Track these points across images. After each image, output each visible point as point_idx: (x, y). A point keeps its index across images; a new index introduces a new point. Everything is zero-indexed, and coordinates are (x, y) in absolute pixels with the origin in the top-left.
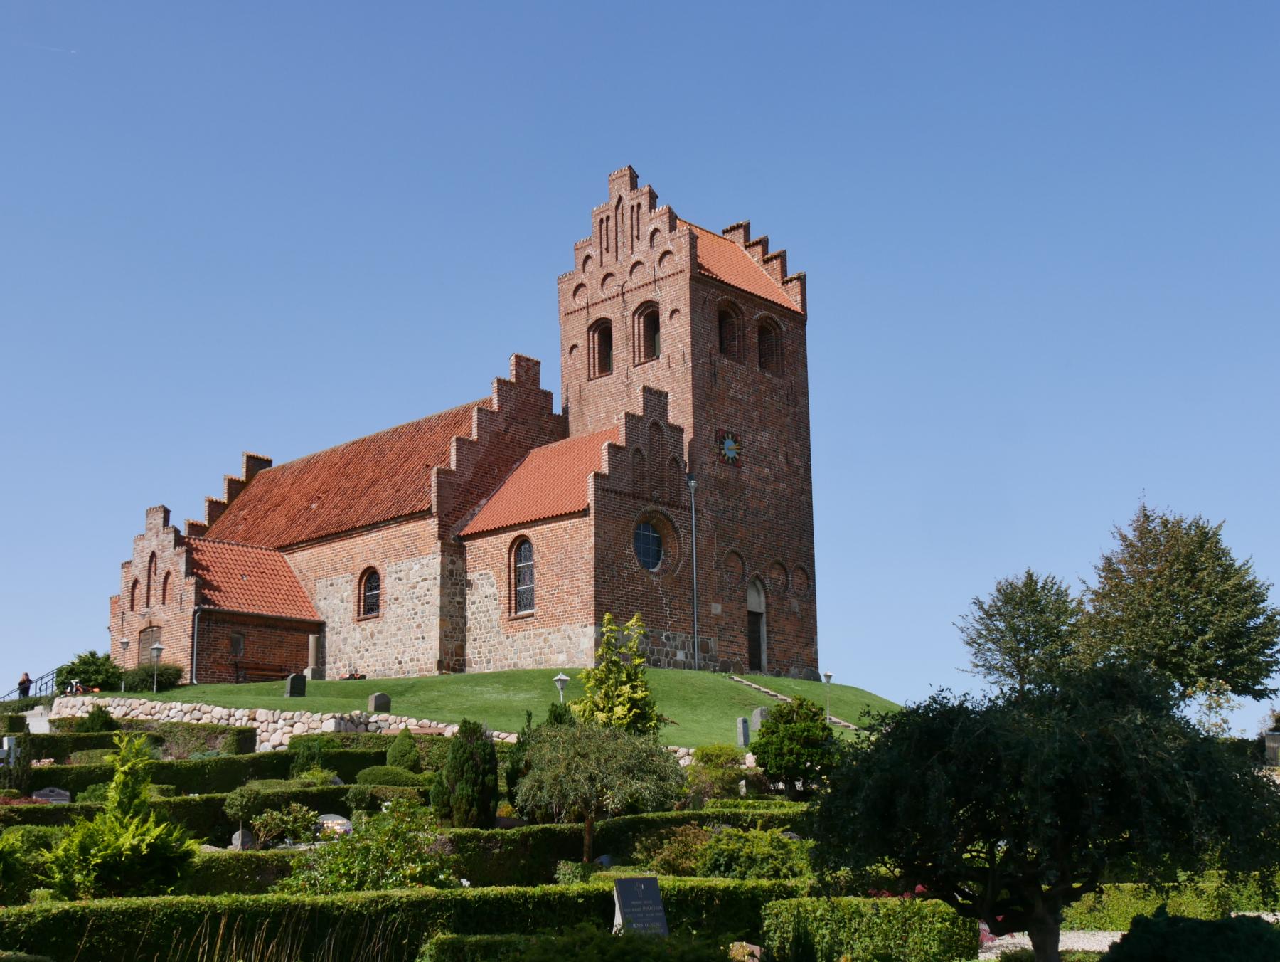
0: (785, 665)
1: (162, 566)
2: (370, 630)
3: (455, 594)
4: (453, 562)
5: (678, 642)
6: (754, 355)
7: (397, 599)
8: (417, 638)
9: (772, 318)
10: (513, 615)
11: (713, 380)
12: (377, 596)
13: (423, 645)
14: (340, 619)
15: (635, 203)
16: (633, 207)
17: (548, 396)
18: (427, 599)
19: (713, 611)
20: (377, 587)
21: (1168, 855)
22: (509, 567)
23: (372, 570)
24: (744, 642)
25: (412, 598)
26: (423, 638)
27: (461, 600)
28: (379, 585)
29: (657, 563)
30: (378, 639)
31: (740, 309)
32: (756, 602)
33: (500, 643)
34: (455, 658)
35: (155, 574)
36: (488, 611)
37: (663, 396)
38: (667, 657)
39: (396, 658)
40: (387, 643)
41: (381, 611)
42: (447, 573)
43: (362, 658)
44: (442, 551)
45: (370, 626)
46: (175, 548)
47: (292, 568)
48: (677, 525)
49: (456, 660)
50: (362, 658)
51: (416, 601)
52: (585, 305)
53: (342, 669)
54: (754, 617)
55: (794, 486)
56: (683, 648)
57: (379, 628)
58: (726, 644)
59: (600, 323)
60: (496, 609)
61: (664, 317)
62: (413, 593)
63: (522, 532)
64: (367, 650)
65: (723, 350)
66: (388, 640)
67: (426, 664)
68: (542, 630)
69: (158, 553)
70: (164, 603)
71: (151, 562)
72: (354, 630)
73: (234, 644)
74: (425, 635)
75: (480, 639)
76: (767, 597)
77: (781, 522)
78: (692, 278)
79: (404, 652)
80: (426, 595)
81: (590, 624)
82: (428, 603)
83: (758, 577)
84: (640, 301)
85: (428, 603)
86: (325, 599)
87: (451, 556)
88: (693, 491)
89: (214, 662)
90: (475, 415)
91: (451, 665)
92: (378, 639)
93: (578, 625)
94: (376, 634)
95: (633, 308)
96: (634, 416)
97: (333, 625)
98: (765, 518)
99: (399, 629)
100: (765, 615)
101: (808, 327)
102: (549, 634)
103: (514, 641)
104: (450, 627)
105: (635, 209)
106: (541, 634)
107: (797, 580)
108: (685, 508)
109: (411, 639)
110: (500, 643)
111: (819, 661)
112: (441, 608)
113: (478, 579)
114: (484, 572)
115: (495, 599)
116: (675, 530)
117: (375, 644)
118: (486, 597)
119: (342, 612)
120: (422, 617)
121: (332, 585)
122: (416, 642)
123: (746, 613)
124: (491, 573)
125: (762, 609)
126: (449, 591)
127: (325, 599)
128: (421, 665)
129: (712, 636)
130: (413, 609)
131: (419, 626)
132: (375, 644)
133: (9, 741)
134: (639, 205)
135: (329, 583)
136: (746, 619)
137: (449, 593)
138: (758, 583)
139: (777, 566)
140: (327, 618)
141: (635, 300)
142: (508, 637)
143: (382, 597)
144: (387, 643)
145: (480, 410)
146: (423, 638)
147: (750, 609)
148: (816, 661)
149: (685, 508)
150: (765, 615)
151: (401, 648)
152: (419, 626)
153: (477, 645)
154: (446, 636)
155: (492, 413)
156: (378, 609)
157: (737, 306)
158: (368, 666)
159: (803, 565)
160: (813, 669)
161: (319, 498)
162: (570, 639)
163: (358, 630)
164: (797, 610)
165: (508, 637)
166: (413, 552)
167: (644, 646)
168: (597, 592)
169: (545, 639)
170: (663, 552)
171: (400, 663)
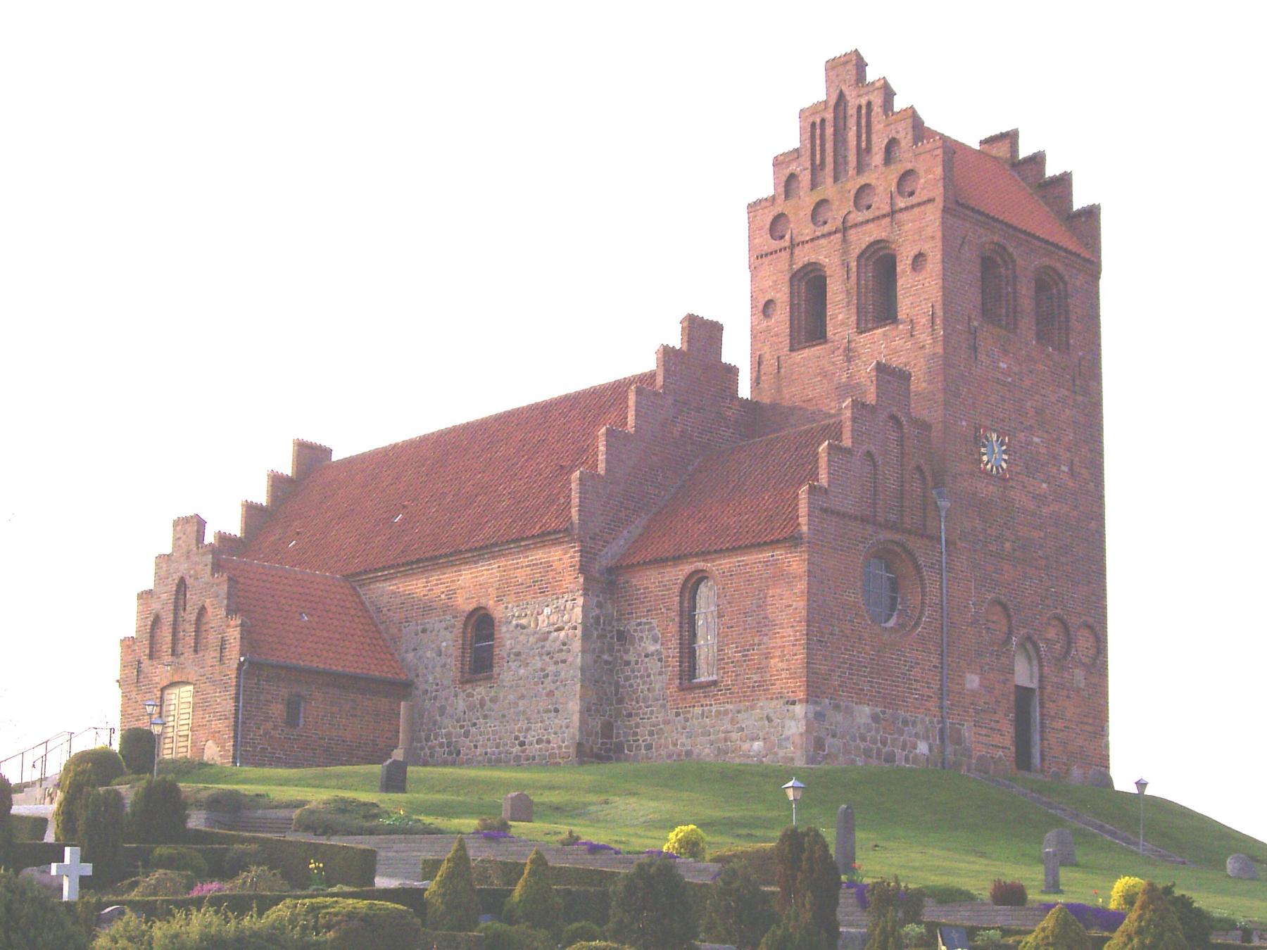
0: (1064, 764)
1: (193, 598)
2: (479, 697)
3: (602, 651)
4: (599, 605)
5: (920, 728)
6: (1027, 325)
7: (518, 654)
8: (547, 711)
9: (1055, 270)
10: (686, 683)
11: (973, 356)
12: (491, 647)
13: (556, 721)
14: (435, 679)
15: (863, 101)
16: (860, 108)
17: (732, 371)
18: (563, 656)
19: (968, 686)
20: (491, 636)
21: (310, 866)
22: (681, 615)
23: (482, 612)
24: (1009, 729)
25: (541, 655)
26: (556, 711)
27: (610, 659)
28: (492, 634)
29: (892, 615)
30: (491, 710)
31: (1010, 255)
32: (1023, 674)
33: (667, 722)
34: (600, 741)
35: (185, 609)
36: (649, 676)
37: (903, 377)
38: (904, 749)
39: (517, 738)
40: (504, 716)
41: (496, 670)
42: (592, 621)
43: (466, 735)
44: (584, 589)
45: (480, 691)
46: (213, 575)
47: (368, 605)
48: (921, 561)
49: (603, 744)
50: (466, 735)
51: (547, 658)
52: (797, 251)
53: (437, 749)
54: (1023, 695)
55: (1081, 508)
56: (926, 738)
57: (493, 694)
58: (984, 732)
59: (810, 268)
60: (661, 673)
61: (903, 265)
62: (543, 647)
63: (700, 565)
64: (475, 724)
65: (988, 312)
66: (506, 712)
67: (560, 747)
68: (730, 707)
69: (189, 581)
70: (196, 651)
71: (178, 591)
72: (456, 696)
73: (293, 708)
74: (560, 707)
75: (637, 714)
76: (1041, 666)
77: (1063, 560)
78: (945, 210)
79: (528, 729)
80: (561, 650)
81: (800, 701)
82: (564, 661)
83: (1029, 638)
84: (868, 239)
85: (564, 661)
86: (415, 650)
87: (598, 596)
88: (943, 514)
89: (265, 734)
90: (632, 398)
91: (595, 750)
92: (491, 710)
93: (782, 701)
94: (488, 703)
95: (858, 251)
96: (863, 405)
97: (427, 687)
98: (1040, 553)
99: (522, 697)
100: (1037, 692)
101: (1101, 282)
102: (739, 712)
103: (687, 720)
104: (595, 696)
105: (864, 111)
106: (726, 712)
107: (1083, 643)
108: (931, 538)
109: (539, 712)
110: (667, 722)
111: (1111, 758)
112: (583, 669)
113: (635, 631)
114: (644, 620)
115: (660, 660)
116: (918, 569)
117: (486, 717)
118: (646, 656)
119: (438, 669)
120: (554, 682)
121: (424, 631)
122: (546, 716)
123: (1013, 689)
124: (655, 622)
125: (1034, 684)
126: (593, 646)
127: (415, 650)
128: (553, 748)
129: (965, 720)
130: (543, 670)
131: (550, 694)
132: (486, 717)
133: (71, 852)
134: (869, 104)
135: (420, 628)
136: (1012, 698)
137: (594, 649)
138: (1029, 646)
139: (1054, 622)
140: (417, 676)
141: (861, 239)
142: (678, 714)
143: (497, 651)
144: (504, 716)
145: (639, 392)
146: (556, 711)
147: (1020, 684)
148: (1106, 758)
149: (931, 538)
150: (1037, 692)
151: (523, 724)
152: (550, 694)
153: (633, 723)
154: (589, 710)
155: (656, 394)
156: (491, 667)
157: (1005, 249)
158: (476, 747)
159: (1091, 620)
160: (1103, 769)
161: (404, 507)
162: (769, 719)
163: (462, 695)
164: (1082, 686)
165: (678, 714)
166: (543, 588)
167: (873, 733)
168: (810, 655)
169: (732, 720)
170: (899, 599)
171: (522, 744)
